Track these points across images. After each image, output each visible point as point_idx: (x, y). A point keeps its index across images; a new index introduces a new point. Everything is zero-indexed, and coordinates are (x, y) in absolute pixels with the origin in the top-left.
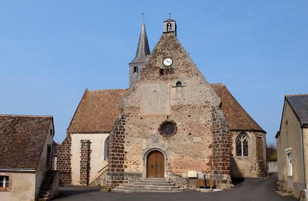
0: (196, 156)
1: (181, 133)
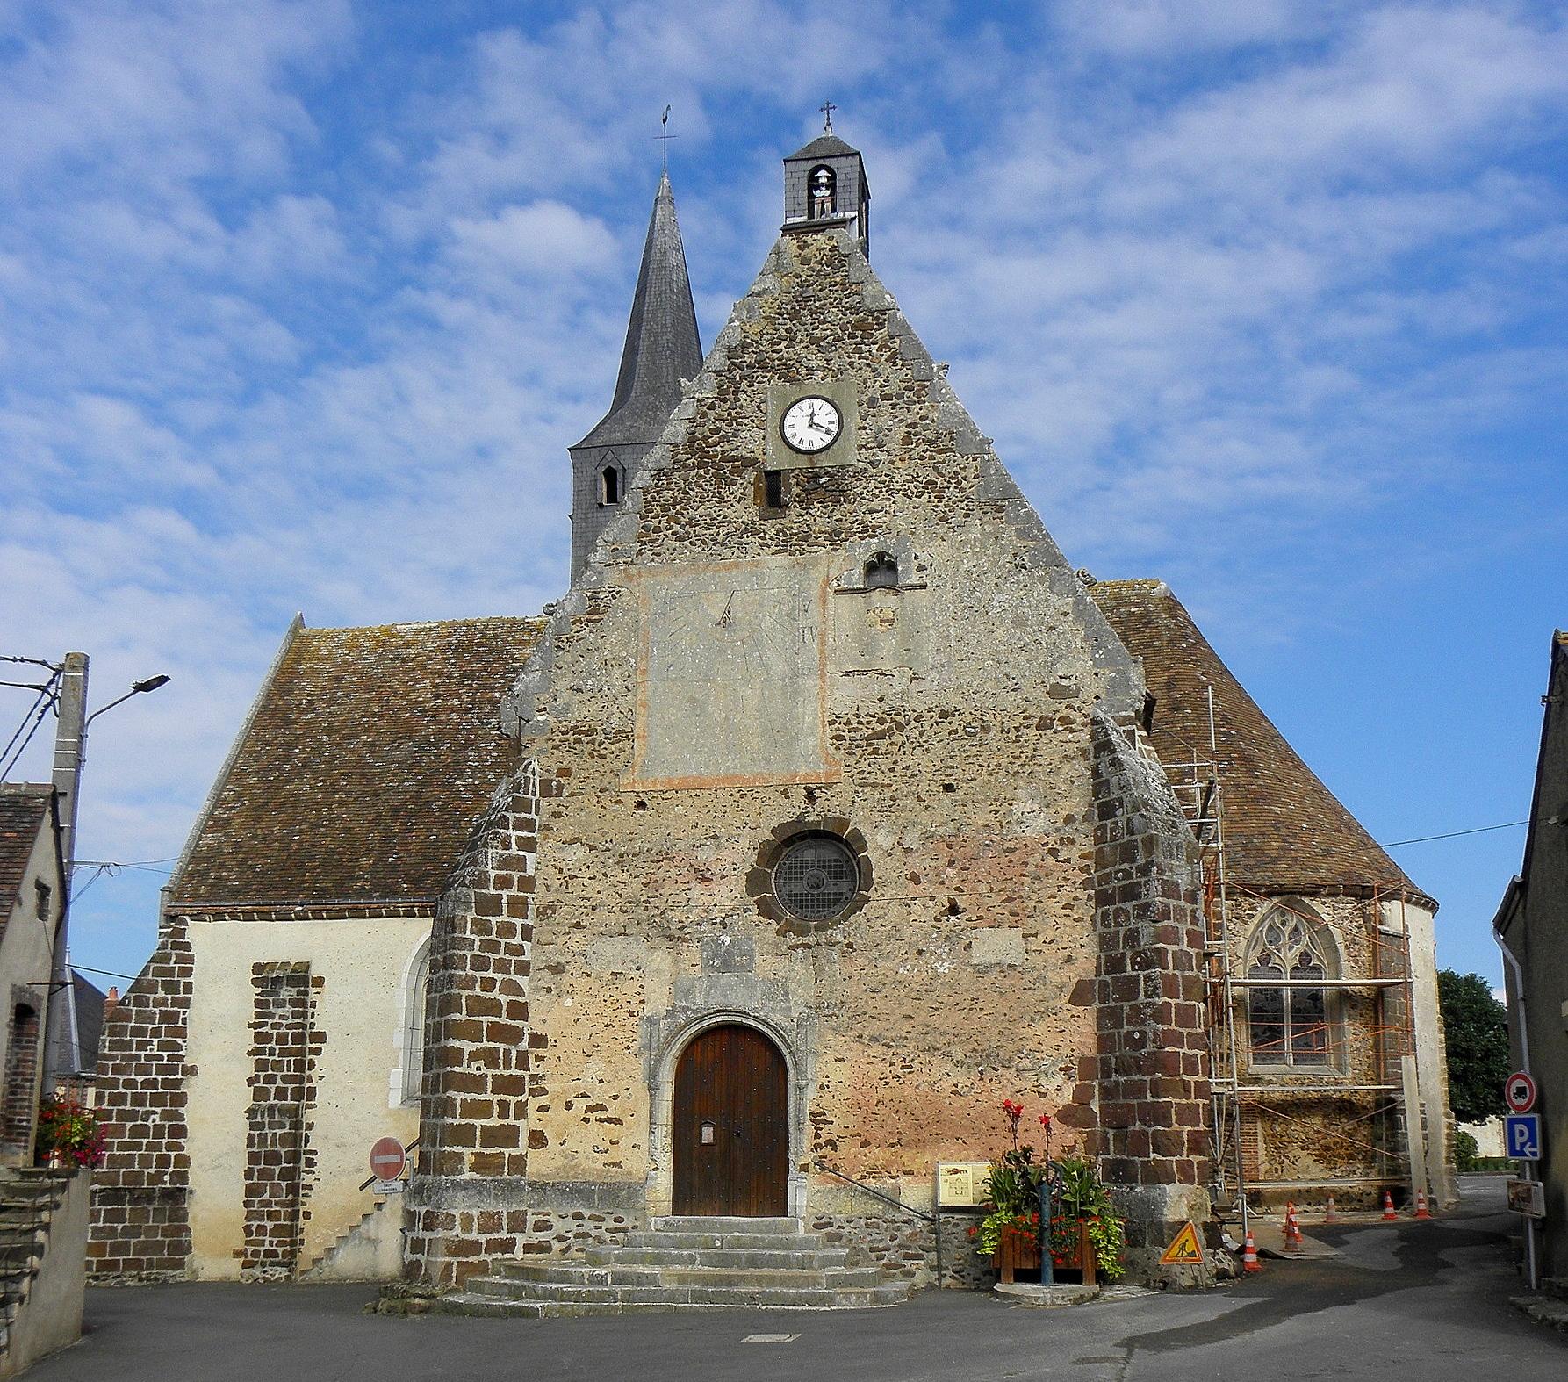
1: (894, 907)
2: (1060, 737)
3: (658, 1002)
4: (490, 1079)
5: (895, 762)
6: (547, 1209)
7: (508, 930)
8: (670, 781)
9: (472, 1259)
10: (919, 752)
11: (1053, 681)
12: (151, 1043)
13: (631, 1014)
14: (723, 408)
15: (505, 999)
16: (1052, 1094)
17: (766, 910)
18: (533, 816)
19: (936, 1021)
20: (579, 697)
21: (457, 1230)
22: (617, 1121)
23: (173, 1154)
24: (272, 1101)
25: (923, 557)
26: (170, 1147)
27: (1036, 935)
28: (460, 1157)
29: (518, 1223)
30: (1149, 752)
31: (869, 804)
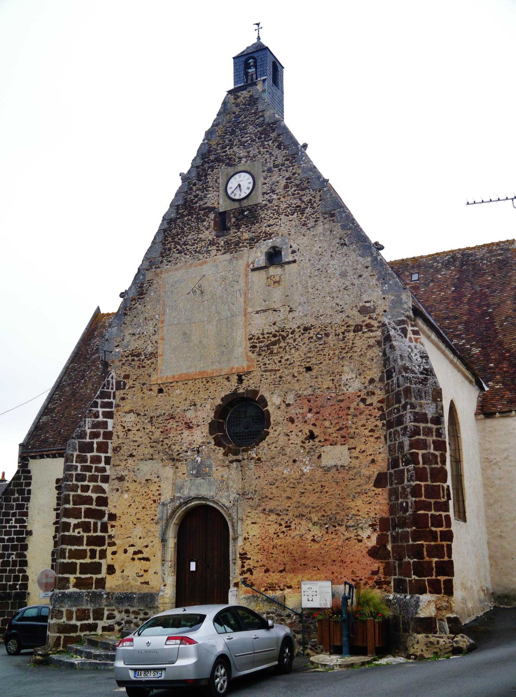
2: (366, 335)
3: (166, 497)
4: (85, 539)
5: (282, 357)
6: (114, 607)
7: (97, 460)
8: (174, 377)
9: (73, 634)
10: (293, 351)
11: (361, 304)
12: (11, 520)
13: (154, 501)
14: (199, 185)
15: (94, 496)
16: (365, 540)
17: (218, 443)
18: (112, 400)
19: (303, 500)
20: (133, 338)
21: (64, 619)
22: (147, 559)
23: (21, 575)
26: (20, 571)
27: (355, 448)
28: (68, 579)
29: (98, 615)
31: (268, 381)
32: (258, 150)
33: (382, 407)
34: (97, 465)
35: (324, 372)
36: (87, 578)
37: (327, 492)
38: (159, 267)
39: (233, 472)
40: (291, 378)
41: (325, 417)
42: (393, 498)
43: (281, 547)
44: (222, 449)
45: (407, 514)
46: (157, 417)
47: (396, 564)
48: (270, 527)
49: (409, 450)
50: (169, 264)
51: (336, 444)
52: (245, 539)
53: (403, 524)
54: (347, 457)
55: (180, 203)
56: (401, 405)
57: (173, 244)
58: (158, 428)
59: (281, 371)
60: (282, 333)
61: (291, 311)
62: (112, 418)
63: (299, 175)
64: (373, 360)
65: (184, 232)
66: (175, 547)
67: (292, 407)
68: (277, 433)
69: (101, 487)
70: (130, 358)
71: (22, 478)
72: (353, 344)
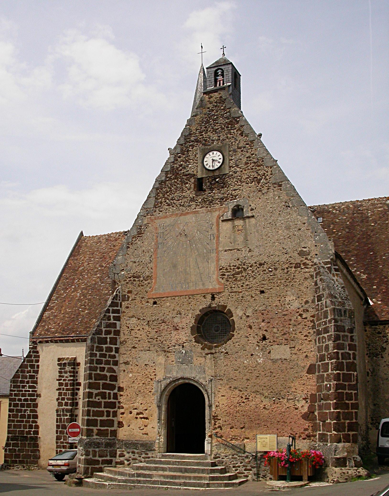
0: (278, 397)
1: (243, 336)
2: (303, 271)
4: (103, 404)
5: (243, 283)
6: (123, 449)
7: (110, 349)
8: (164, 293)
9: (96, 466)
10: (251, 279)
11: (300, 249)
13: (151, 379)
15: (108, 374)
16: (300, 408)
22: (147, 418)
23: (34, 424)
24: (64, 407)
25: (253, 205)
27: (294, 347)
28: (92, 430)
30: (337, 275)
32: (226, 136)
33: (313, 320)
34: (110, 353)
35: (274, 295)
36: (105, 430)
37: (274, 376)
38: (153, 215)
39: (208, 361)
40: (250, 297)
41: (274, 326)
42: (320, 381)
43: (242, 412)
44: (200, 345)
45: (330, 392)
46: (153, 321)
47: (321, 424)
48: (235, 399)
49: (333, 350)
50: (161, 213)
51: (281, 344)
52: (217, 406)
53: (326, 398)
54: (289, 353)
55: (169, 169)
56: (327, 320)
57: (164, 198)
58: (154, 329)
59: (243, 293)
60: (244, 266)
61: (250, 251)
62: (119, 320)
63: (256, 155)
64: (307, 288)
65: (171, 191)
66: (166, 411)
67: (250, 318)
68: (239, 335)
69: (112, 368)
70: (132, 279)
71: (33, 356)
72: (294, 276)
